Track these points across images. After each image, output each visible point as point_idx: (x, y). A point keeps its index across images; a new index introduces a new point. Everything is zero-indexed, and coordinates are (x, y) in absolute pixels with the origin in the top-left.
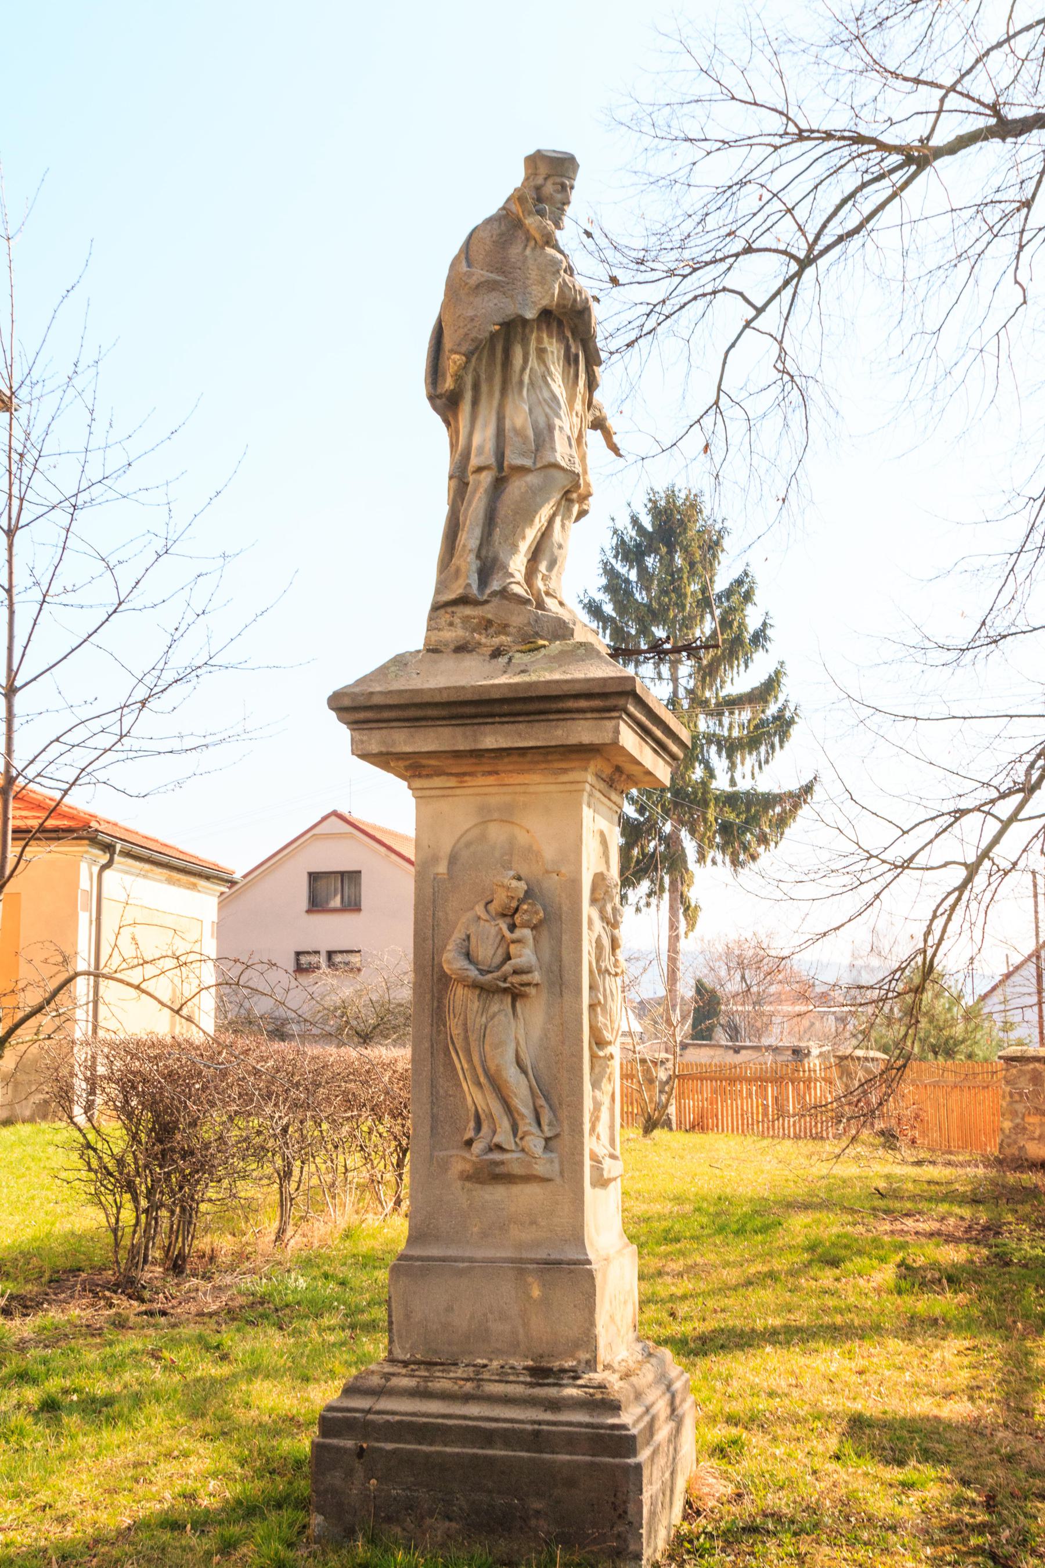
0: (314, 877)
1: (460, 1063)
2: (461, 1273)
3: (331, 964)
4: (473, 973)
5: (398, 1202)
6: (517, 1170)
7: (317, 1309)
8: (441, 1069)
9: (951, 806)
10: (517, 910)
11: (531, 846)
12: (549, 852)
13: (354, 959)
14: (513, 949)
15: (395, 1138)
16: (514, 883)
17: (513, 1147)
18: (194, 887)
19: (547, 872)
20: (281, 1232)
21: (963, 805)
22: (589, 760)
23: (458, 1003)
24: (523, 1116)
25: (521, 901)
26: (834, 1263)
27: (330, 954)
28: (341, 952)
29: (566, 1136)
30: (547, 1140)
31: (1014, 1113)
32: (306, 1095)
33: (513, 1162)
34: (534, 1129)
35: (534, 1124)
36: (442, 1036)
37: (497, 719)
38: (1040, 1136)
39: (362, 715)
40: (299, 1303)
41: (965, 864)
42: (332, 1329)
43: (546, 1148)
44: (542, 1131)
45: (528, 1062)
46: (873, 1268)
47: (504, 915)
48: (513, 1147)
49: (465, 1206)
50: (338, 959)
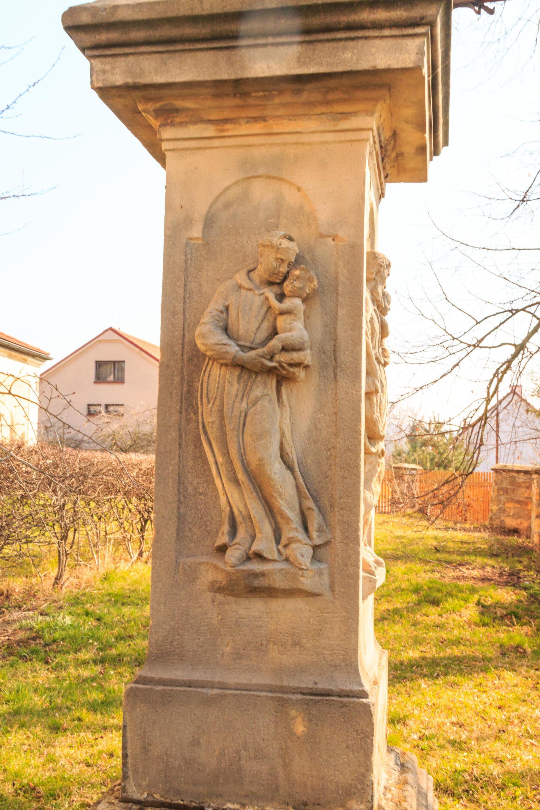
0: (99, 364)
1: (213, 456)
2: (210, 701)
3: (107, 412)
4: (233, 349)
5: (141, 554)
6: (279, 582)
7: (77, 644)
8: (191, 463)
9: (508, 307)
10: (286, 277)
11: (301, 207)
12: (324, 213)
13: (120, 409)
14: (281, 322)
15: (140, 512)
16: (285, 243)
17: (276, 556)
18: (25, 361)
19: (321, 236)
20: (58, 578)
21: (515, 306)
22: (376, 100)
23: (213, 385)
24: (288, 520)
25: (293, 265)
26: (435, 603)
27: (107, 406)
28: (113, 405)
29: (338, 545)
30: (316, 548)
31: (499, 501)
32: (80, 483)
33: (274, 571)
34: (301, 535)
35: (301, 530)
36: (192, 426)
37: (271, 40)
38: (513, 515)
39: (104, 37)
40: (63, 640)
41: (514, 345)
42: (85, 663)
43: (315, 558)
44: (310, 537)
45: (293, 456)
46: (461, 606)
47: (271, 284)
48: (276, 556)
49: (215, 622)
50: (111, 409)
